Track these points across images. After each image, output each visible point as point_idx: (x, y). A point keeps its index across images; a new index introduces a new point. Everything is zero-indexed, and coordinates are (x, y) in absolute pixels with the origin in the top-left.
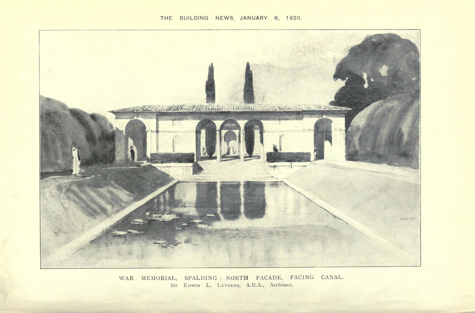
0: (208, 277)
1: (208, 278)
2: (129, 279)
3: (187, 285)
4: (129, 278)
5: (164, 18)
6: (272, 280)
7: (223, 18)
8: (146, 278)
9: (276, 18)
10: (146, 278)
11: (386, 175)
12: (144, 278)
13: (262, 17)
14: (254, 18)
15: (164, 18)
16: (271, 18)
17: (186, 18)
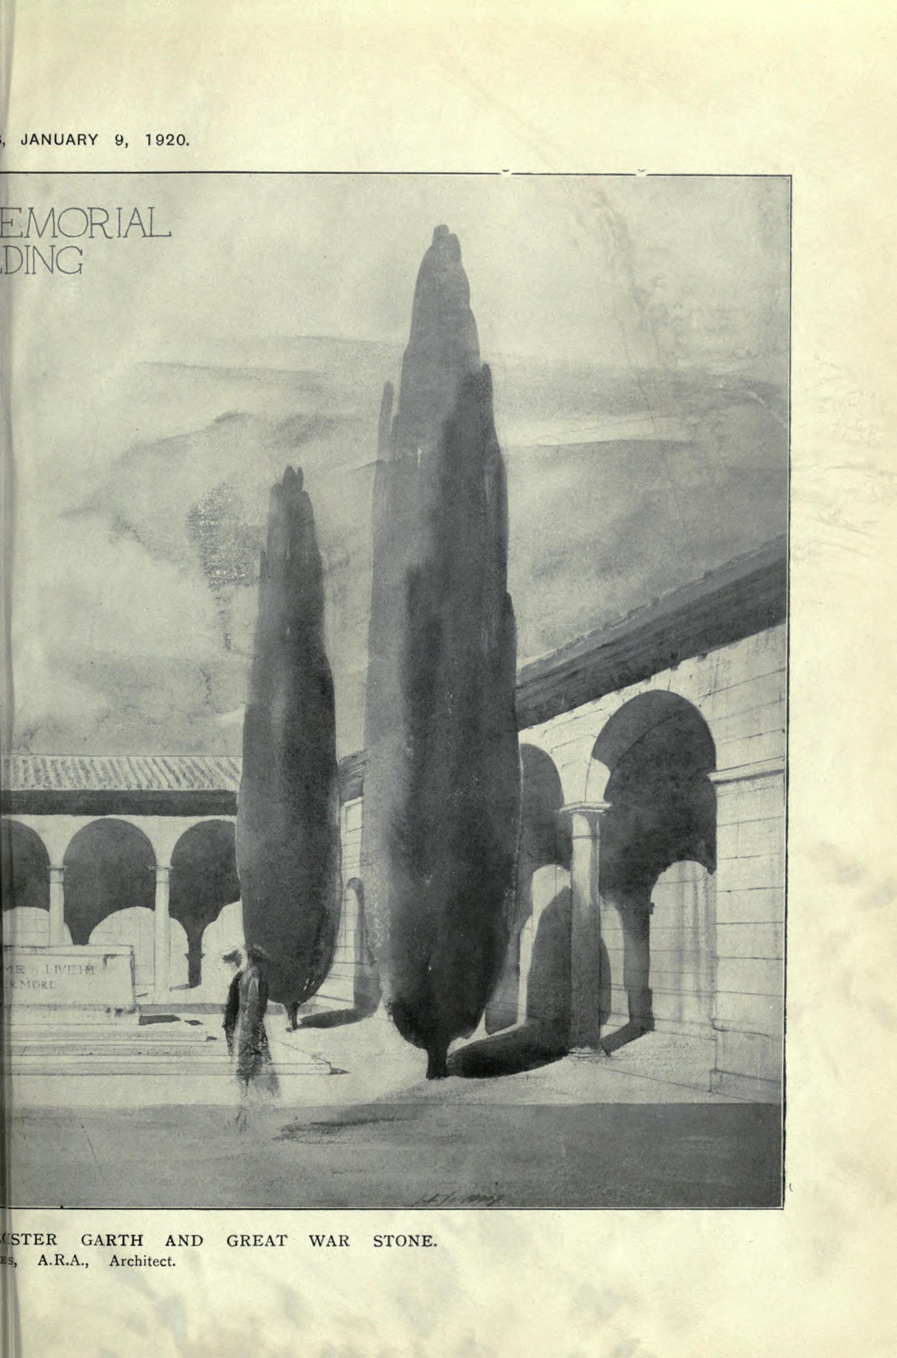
0: (190, 1242)
2: (337, 1242)
6: (338, 1248)
9: (119, 140)
10: (421, 1240)
11: (102, 1061)
12: (316, 1240)
13: (82, 139)
16: (106, 140)
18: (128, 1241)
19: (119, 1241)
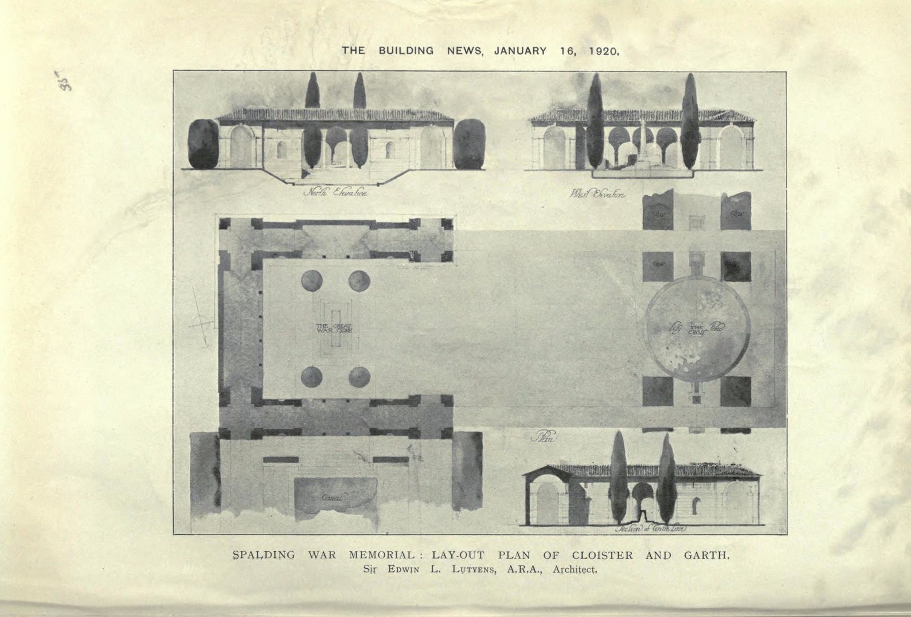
0: (662, 556)
1: (278, 555)
2: (328, 556)
3: (395, 569)
4: (328, 555)
5: (348, 50)
7: (463, 51)
8: (359, 555)
10: (359, 555)
13: (536, 50)
14: (520, 51)
15: (348, 50)
17: (390, 51)
18: (716, 556)
19: (710, 556)
